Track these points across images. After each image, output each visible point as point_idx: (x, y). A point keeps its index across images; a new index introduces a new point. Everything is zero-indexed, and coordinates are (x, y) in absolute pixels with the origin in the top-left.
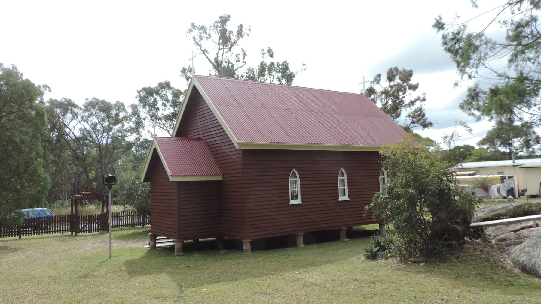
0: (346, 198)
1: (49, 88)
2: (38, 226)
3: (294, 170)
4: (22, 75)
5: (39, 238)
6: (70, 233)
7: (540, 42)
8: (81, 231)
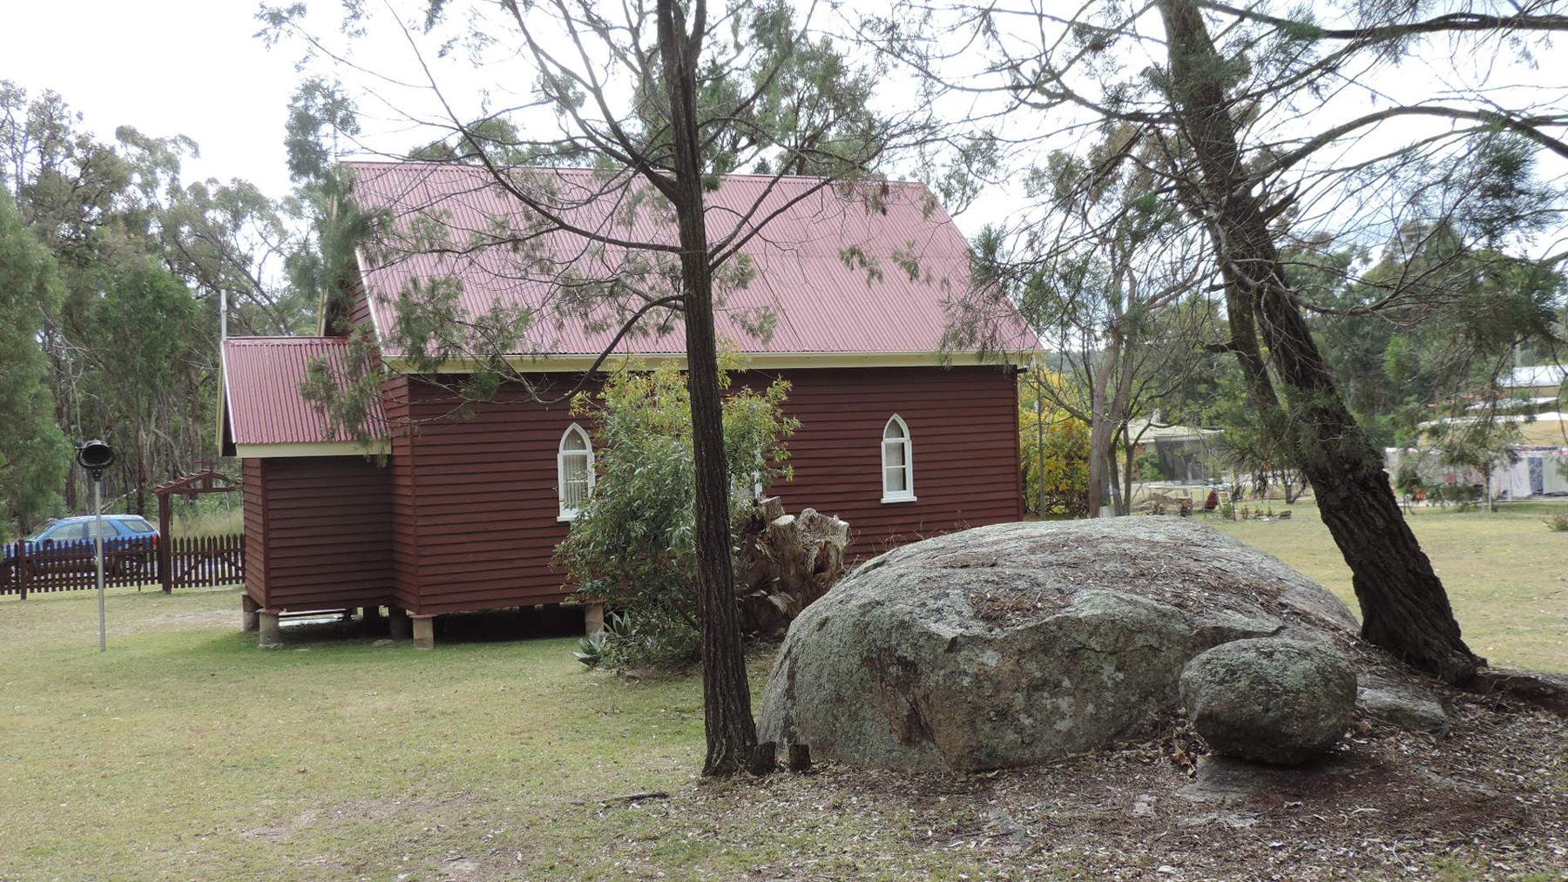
0: (908, 496)
1: (191, 144)
2: (66, 567)
3: (896, 417)
4: (1156, 65)
5: (61, 600)
6: (158, 587)
7: (772, 27)
8: (180, 582)
